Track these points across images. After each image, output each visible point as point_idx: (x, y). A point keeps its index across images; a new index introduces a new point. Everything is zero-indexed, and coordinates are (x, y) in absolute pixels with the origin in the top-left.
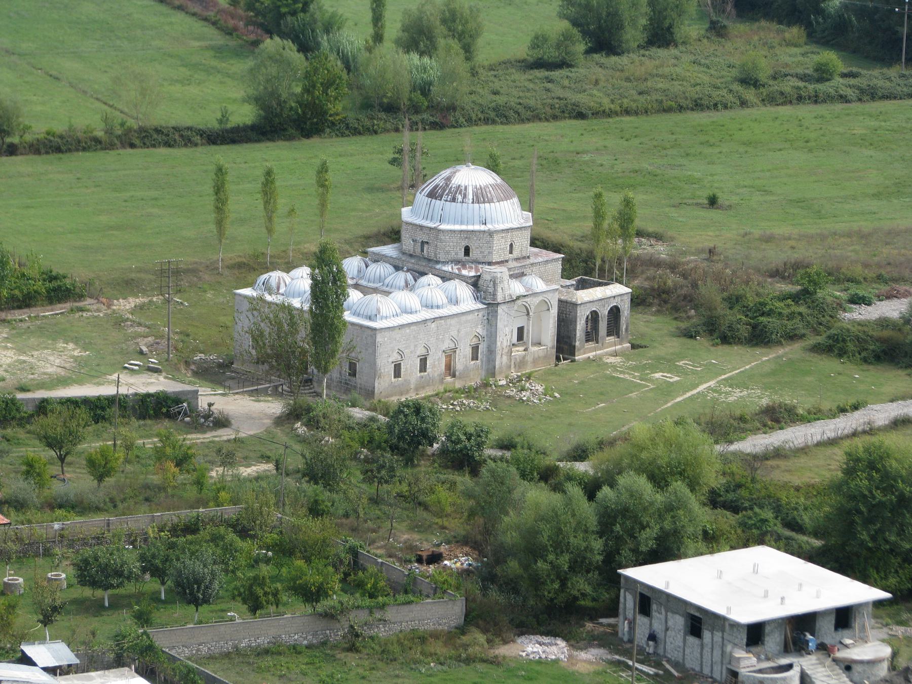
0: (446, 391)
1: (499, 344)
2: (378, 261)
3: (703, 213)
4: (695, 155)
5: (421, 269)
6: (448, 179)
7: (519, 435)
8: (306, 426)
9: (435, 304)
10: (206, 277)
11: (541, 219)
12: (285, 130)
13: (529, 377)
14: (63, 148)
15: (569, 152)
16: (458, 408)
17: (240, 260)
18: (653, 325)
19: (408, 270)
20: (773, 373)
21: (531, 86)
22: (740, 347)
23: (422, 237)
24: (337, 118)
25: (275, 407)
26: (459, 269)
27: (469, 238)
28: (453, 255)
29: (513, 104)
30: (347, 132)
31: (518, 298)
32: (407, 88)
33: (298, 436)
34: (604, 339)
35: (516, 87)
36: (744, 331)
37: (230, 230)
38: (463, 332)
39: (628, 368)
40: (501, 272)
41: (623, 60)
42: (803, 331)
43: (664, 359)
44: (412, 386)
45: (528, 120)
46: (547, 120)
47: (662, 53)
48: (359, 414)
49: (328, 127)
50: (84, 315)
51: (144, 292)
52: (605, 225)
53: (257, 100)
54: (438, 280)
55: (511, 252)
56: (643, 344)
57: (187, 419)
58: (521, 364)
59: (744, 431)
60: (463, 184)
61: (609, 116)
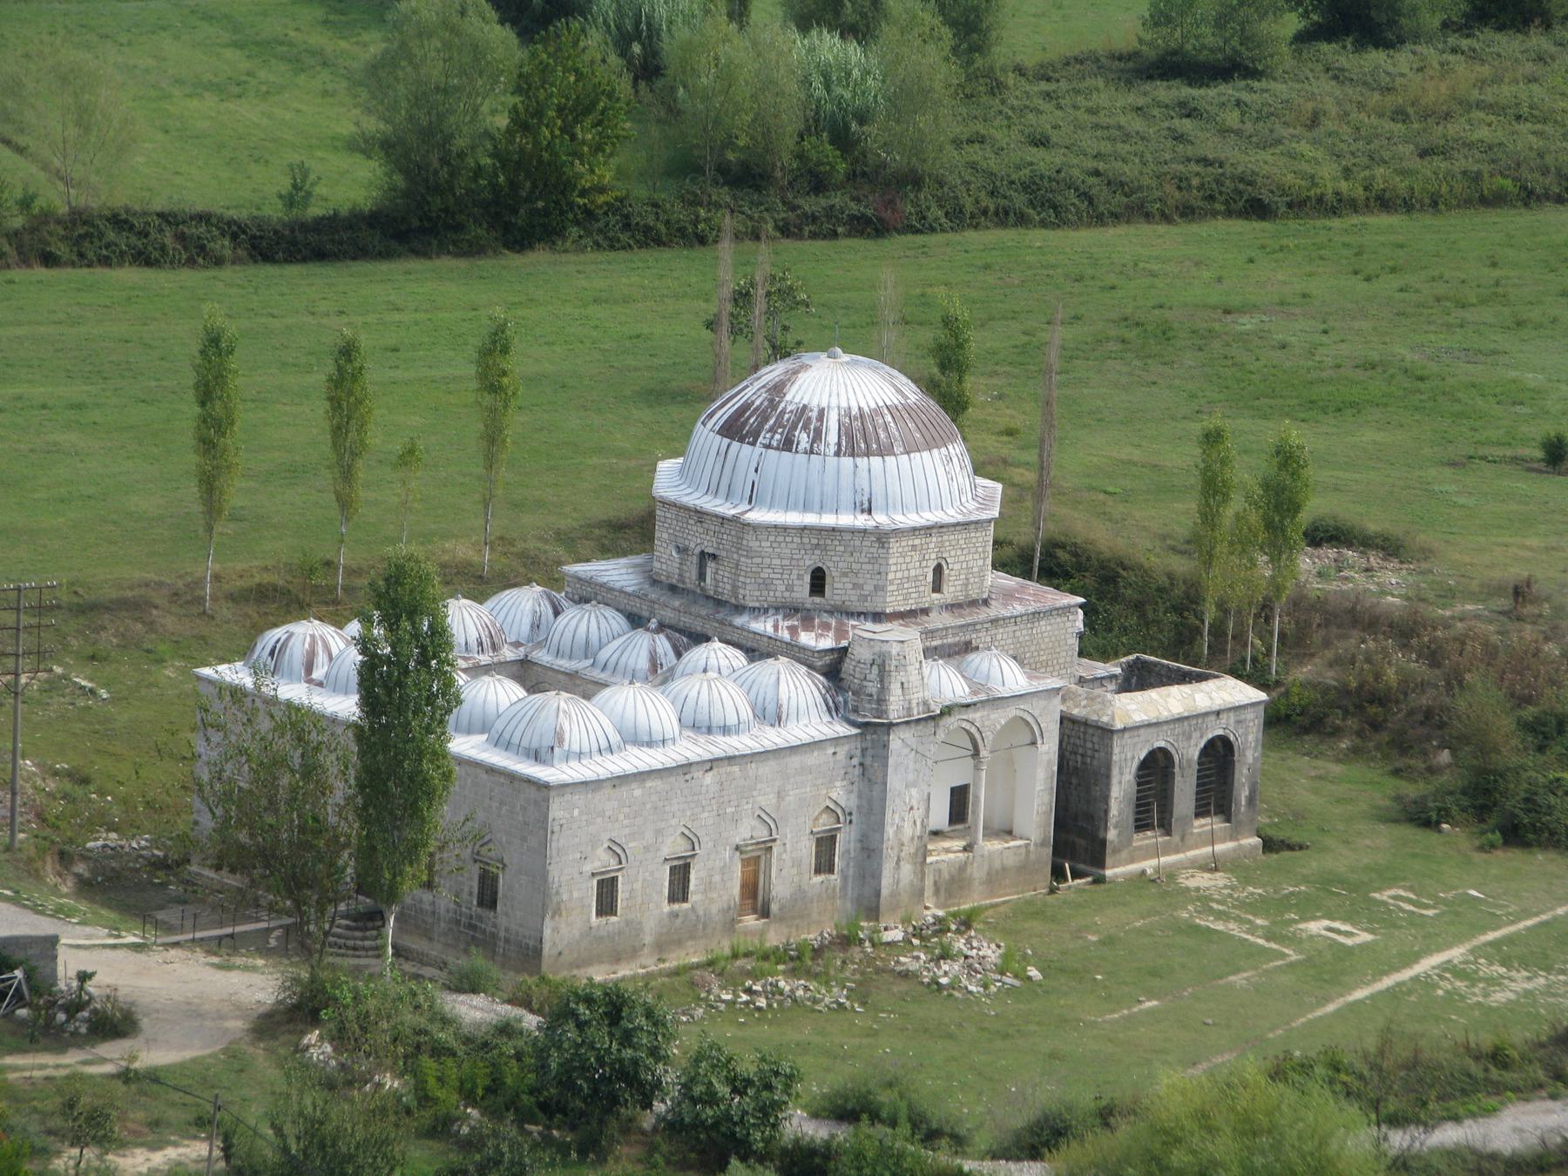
0: (735, 956)
1: (890, 831)
2: (587, 601)
3: (1524, 485)
4: (1538, 326)
5: (697, 626)
6: (778, 389)
7: (890, 1085)
8: (332, 1040)
9: (717, 720)
10: (169, 622)
11: (1091, 489)
12: (459, 228)
13: (966, 923)
15: (1205, 306)
16: (762, 1002)
17: (267, 578)
18: (1331, 787)
19: (662, 627)
21: (1138, 124)
22: (1552, 855)
23: (700, 540)
24: (601, 199)
25: (258, 985)
26: (793, 630)
27: (825, 549)
28: (779, 592)
29: (1076, 172)
30: (624, 237)
31: (947, 711)
32: (790, 124)
33: (306, 1066)
34: (1186, 823)
35: (1096, 126)
37: (236, 494)
38: (792, 797)
39: (1243, 905)
40: (902, 639)
41: (1398, 63)
43: (1342, 882)
44: (648, 939)
45: (1116, 217)
46: (1166, 218)
47: (1508, 44)
48: (474, 1011)
49: (577, 223)
52: (1229, 513)
53: (388, 147)
54: (737, 658)
55: (937, 587)
56: (1296, 838)
57: (23, 1012)
58: (953, 885)
59: (1498, 1089)
60: (814, 404)
61: (1334, 211)
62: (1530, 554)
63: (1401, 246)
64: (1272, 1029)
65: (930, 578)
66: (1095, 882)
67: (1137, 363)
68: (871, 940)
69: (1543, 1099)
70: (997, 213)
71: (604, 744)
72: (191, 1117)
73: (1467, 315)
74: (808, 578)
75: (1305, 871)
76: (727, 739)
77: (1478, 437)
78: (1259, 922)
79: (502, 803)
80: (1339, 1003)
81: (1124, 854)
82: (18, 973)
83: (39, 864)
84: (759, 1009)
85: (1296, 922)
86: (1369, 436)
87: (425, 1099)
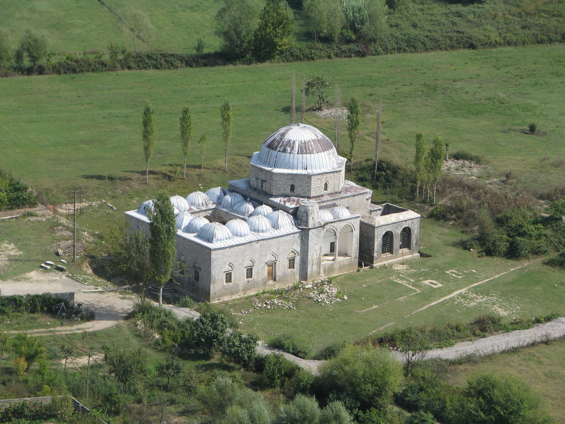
1: (310, 257)
6: (283, 135)
9: (260, 229)
14: (77, 70)
16: (269, 307)
20: (513, 283)
24: (284, 48)
27: (294, 179)
28: (282, 191)
30: (291, 59)
31: (327, 224)
34: (397, 250)
36: (503, 246)
42: (546, 249)
44: (241, 288)
46: (446, 49)
49: (278, 54)
50: (32, 219)
51: (88, 198)
55: (326, 189)
56: (429, 254)
57: (64, 314)
58: (330, 269)
60: (292, 140)
61: (494, 46)
62: (517, 162)
63: (510, 58)
64: (406, 315)
65: (323, 187)
66: (371, 268)
67: (424, 98)
68: (303, 288)
69: (467, 341)
70: (397, 49)
71: (228, 237)
72: (101, 346)
73: (523, 81)
74: (290, 187)
75: (429, 264)
76: (263, 234)
77: (514, 123)
78: (412, 280)
79: (200, 253)
80: (427, 306)
81: (379, 260)
82: (63, 304)
83: (81, 265)
84: (268, 309)
85: (422, 280)
86: (484, 122)
87: (164, 341)
